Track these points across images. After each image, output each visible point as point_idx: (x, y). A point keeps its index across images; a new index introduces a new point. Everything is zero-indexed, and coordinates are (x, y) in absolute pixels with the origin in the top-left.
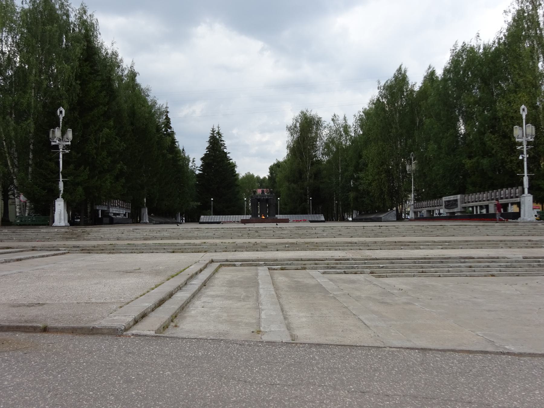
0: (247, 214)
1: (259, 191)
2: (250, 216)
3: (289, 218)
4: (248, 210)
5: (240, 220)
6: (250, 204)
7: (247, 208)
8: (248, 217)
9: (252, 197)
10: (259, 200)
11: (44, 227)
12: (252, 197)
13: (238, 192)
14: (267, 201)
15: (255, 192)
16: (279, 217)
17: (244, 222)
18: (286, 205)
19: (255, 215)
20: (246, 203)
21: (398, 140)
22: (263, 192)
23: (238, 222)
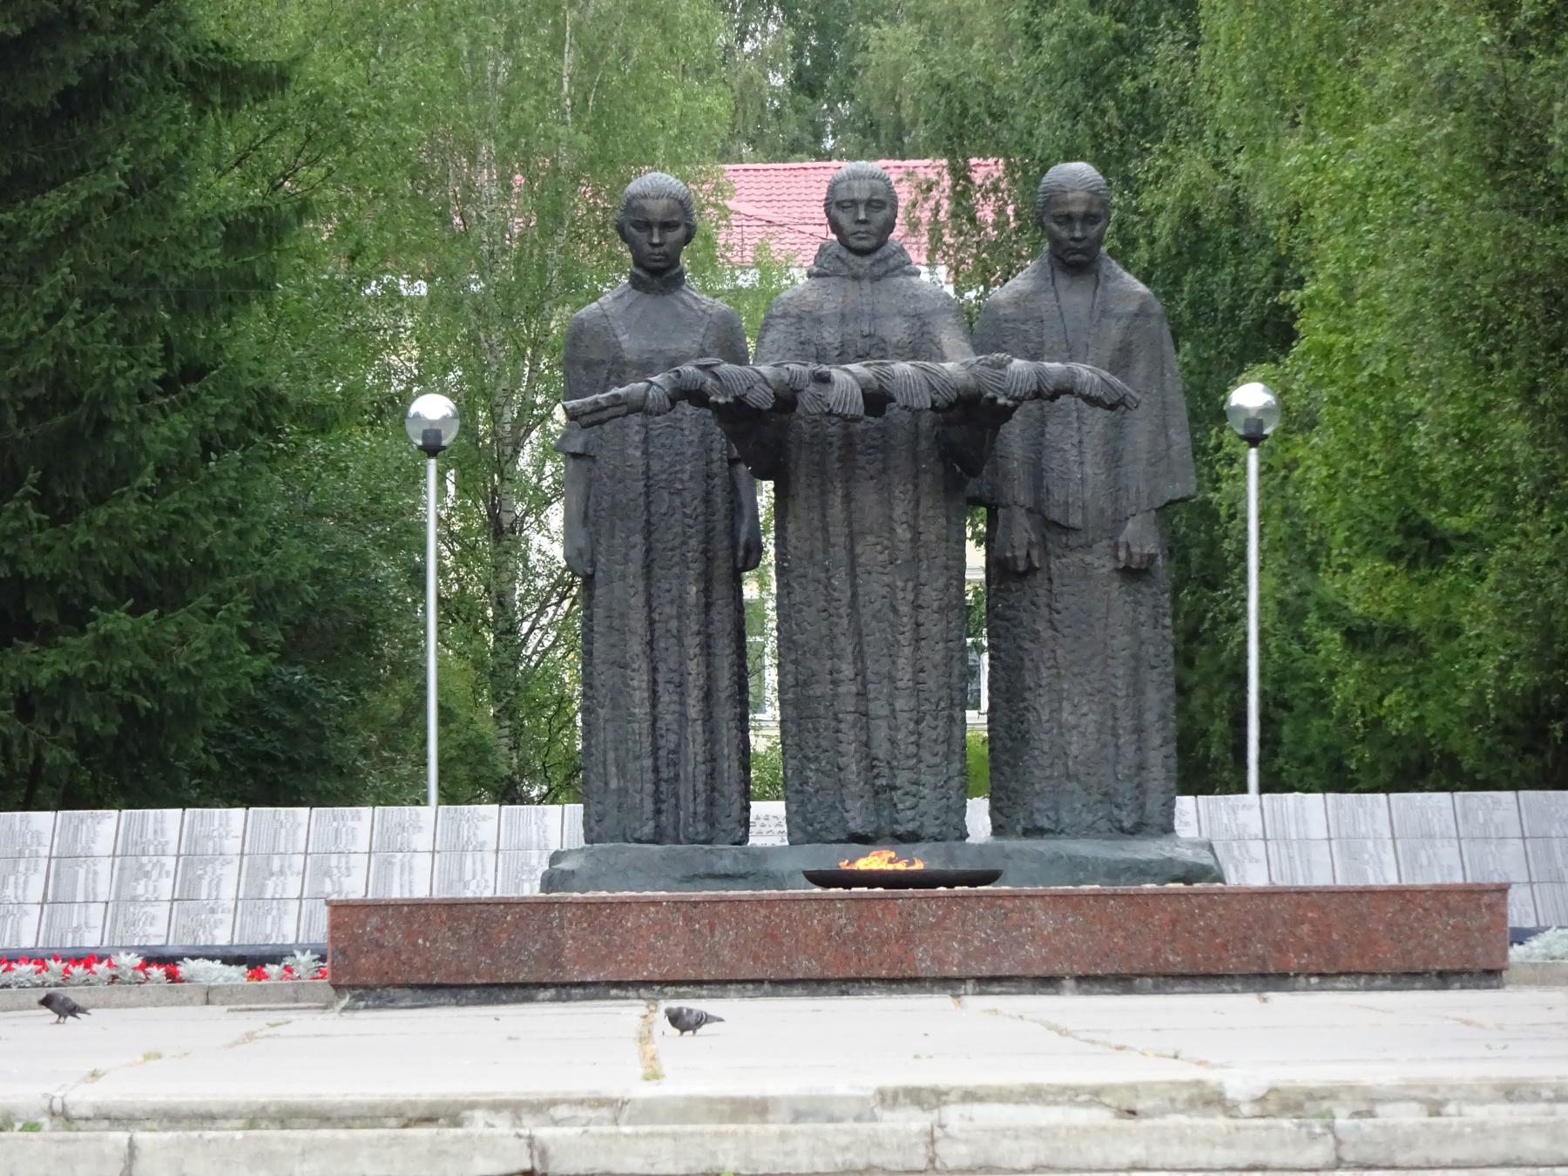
0: (479, 778)
1: (767, 221)
2: (555, 826)
3: (1502, 863)
4: (502, 676)
5: (297, 924)
6: (547, 541)
7: (486, 616)
8: (511, 848)
9: (588, 360)
10: (763, 432)
11: (1097, 988)
12: (588, 360)
13: (258, 232)
14: (964, 442)
15: (660, 248)
16: (1265, 838)
17: (392, 958)
18: (1421, 546)
19: (668, 794)
20: (436, 498)
21: (514, 172)
22: (860, 236)
23: (254, 961)
